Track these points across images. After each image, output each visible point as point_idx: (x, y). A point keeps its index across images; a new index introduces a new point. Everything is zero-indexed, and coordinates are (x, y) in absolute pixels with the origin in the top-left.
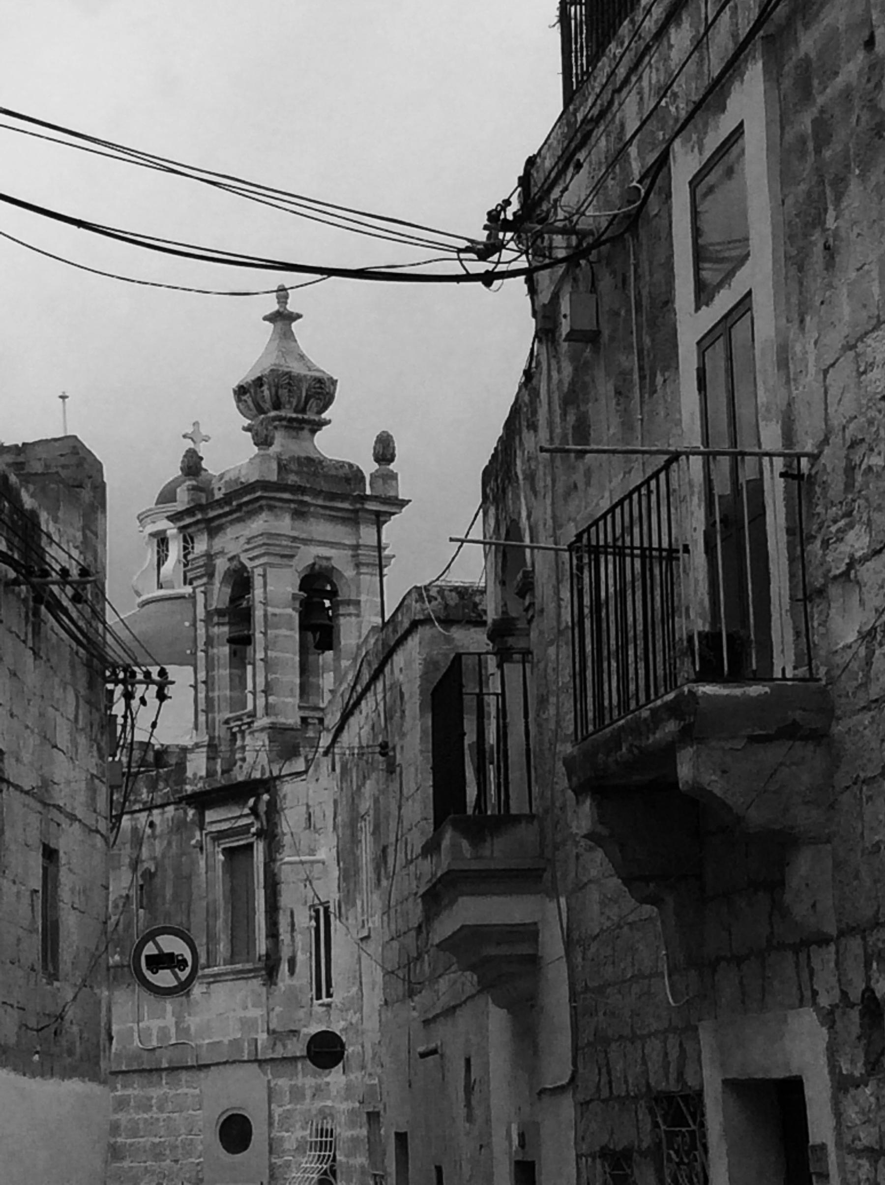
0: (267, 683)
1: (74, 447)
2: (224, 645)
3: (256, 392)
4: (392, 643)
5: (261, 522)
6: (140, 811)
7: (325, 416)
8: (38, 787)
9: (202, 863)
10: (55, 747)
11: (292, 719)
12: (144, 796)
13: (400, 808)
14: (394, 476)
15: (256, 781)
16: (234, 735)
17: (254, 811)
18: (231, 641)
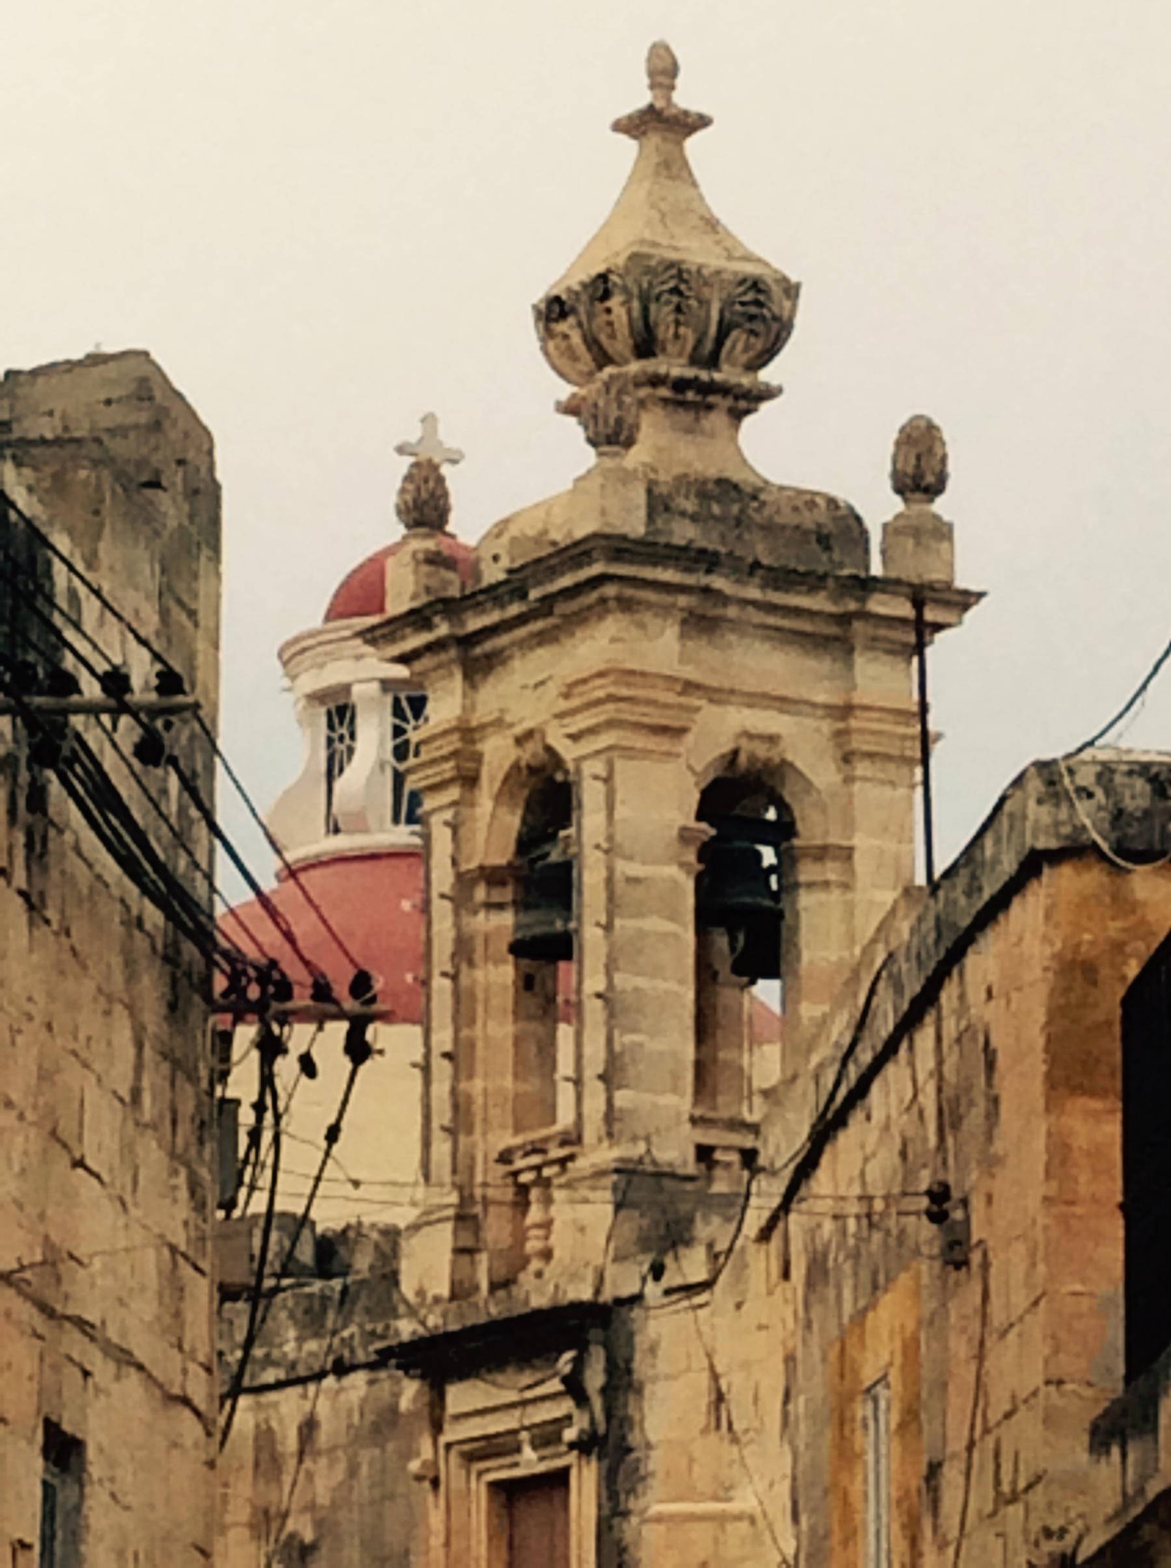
0: (613, 1059)
1: (143, 381)
2: (498, 962)
3: (591, 316)
4: (965, 922)
5: (604, 642)
6: (279, 1385)
7: (768, 375)
8: (32, 1265)
9: (436, 1520)
10: (79, 1163)
11: (675, 1151)
12: (290, 1348)
13: (980, 1357)
14: (943, 532)
15: (577, 1307)
16: (523, 1190)
17: (574, 1387)
18: (518, 949)
